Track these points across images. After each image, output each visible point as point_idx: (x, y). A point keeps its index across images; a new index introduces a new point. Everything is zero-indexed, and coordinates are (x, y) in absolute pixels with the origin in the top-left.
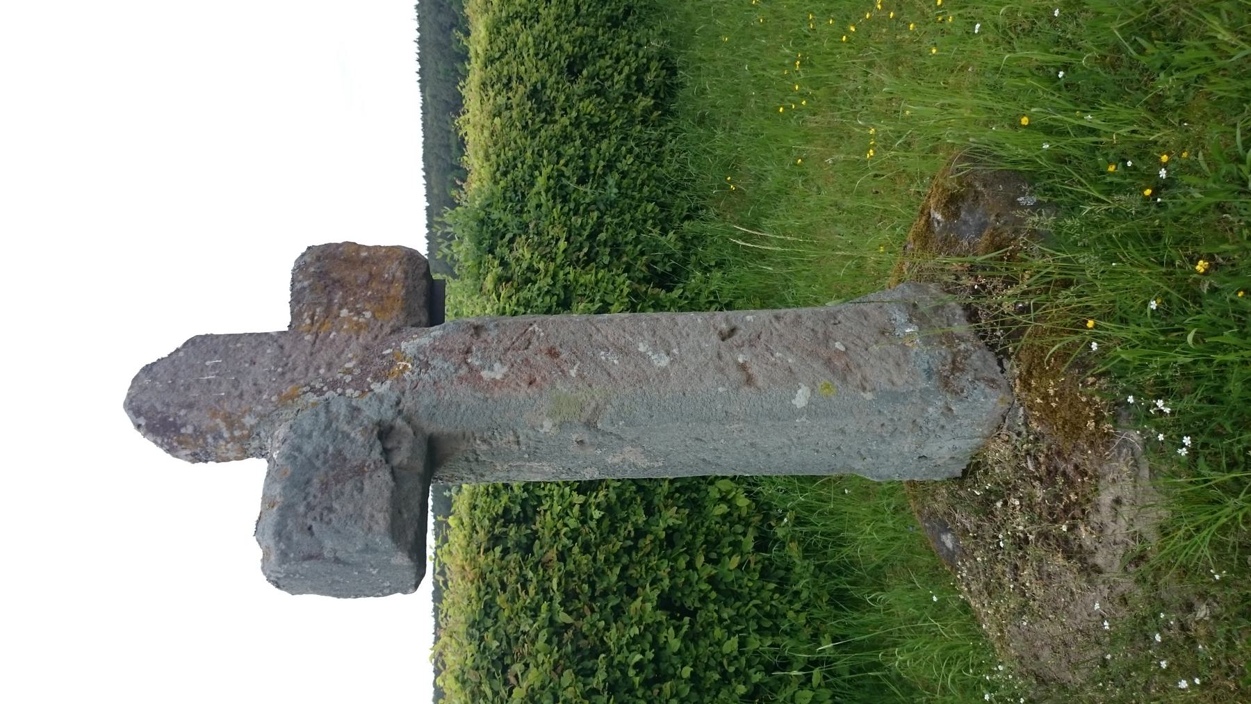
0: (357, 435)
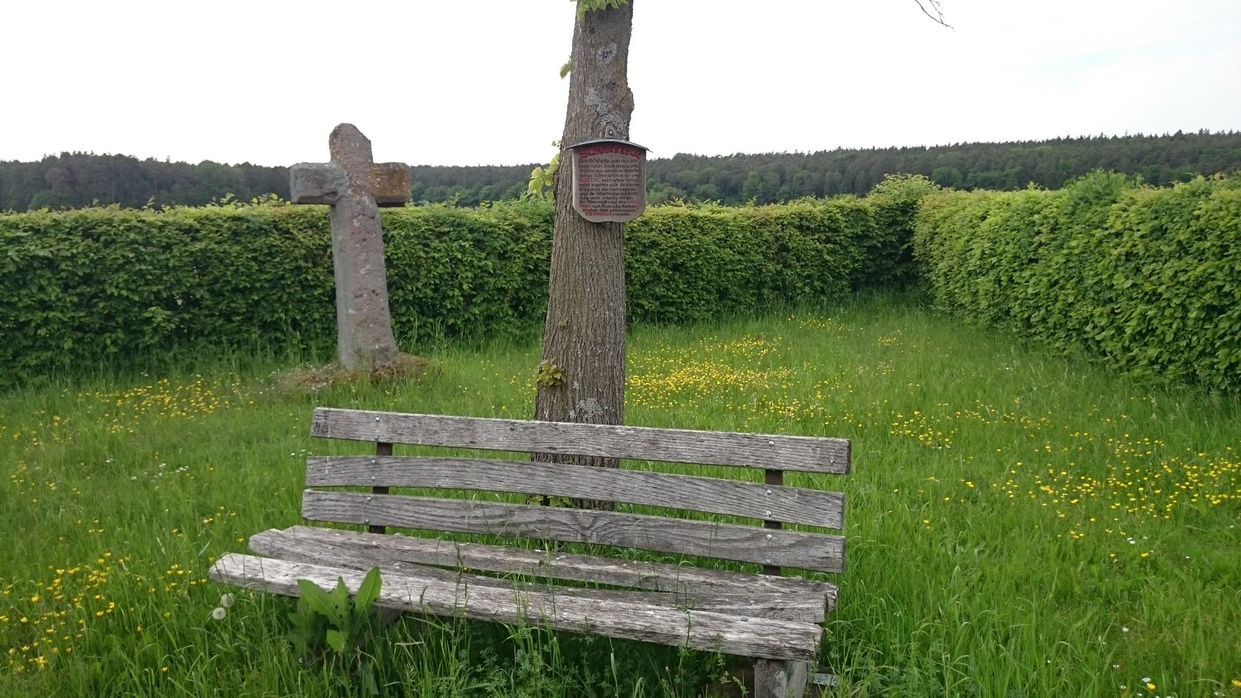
0: (333, 186)
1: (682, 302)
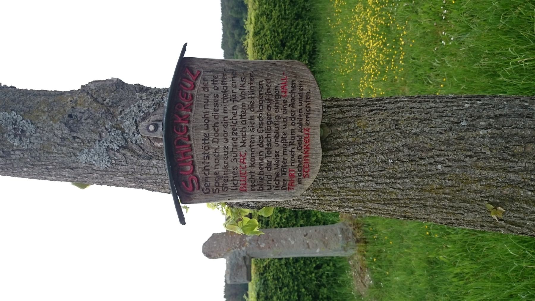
0: (240, 259)
1: (304, 41)
